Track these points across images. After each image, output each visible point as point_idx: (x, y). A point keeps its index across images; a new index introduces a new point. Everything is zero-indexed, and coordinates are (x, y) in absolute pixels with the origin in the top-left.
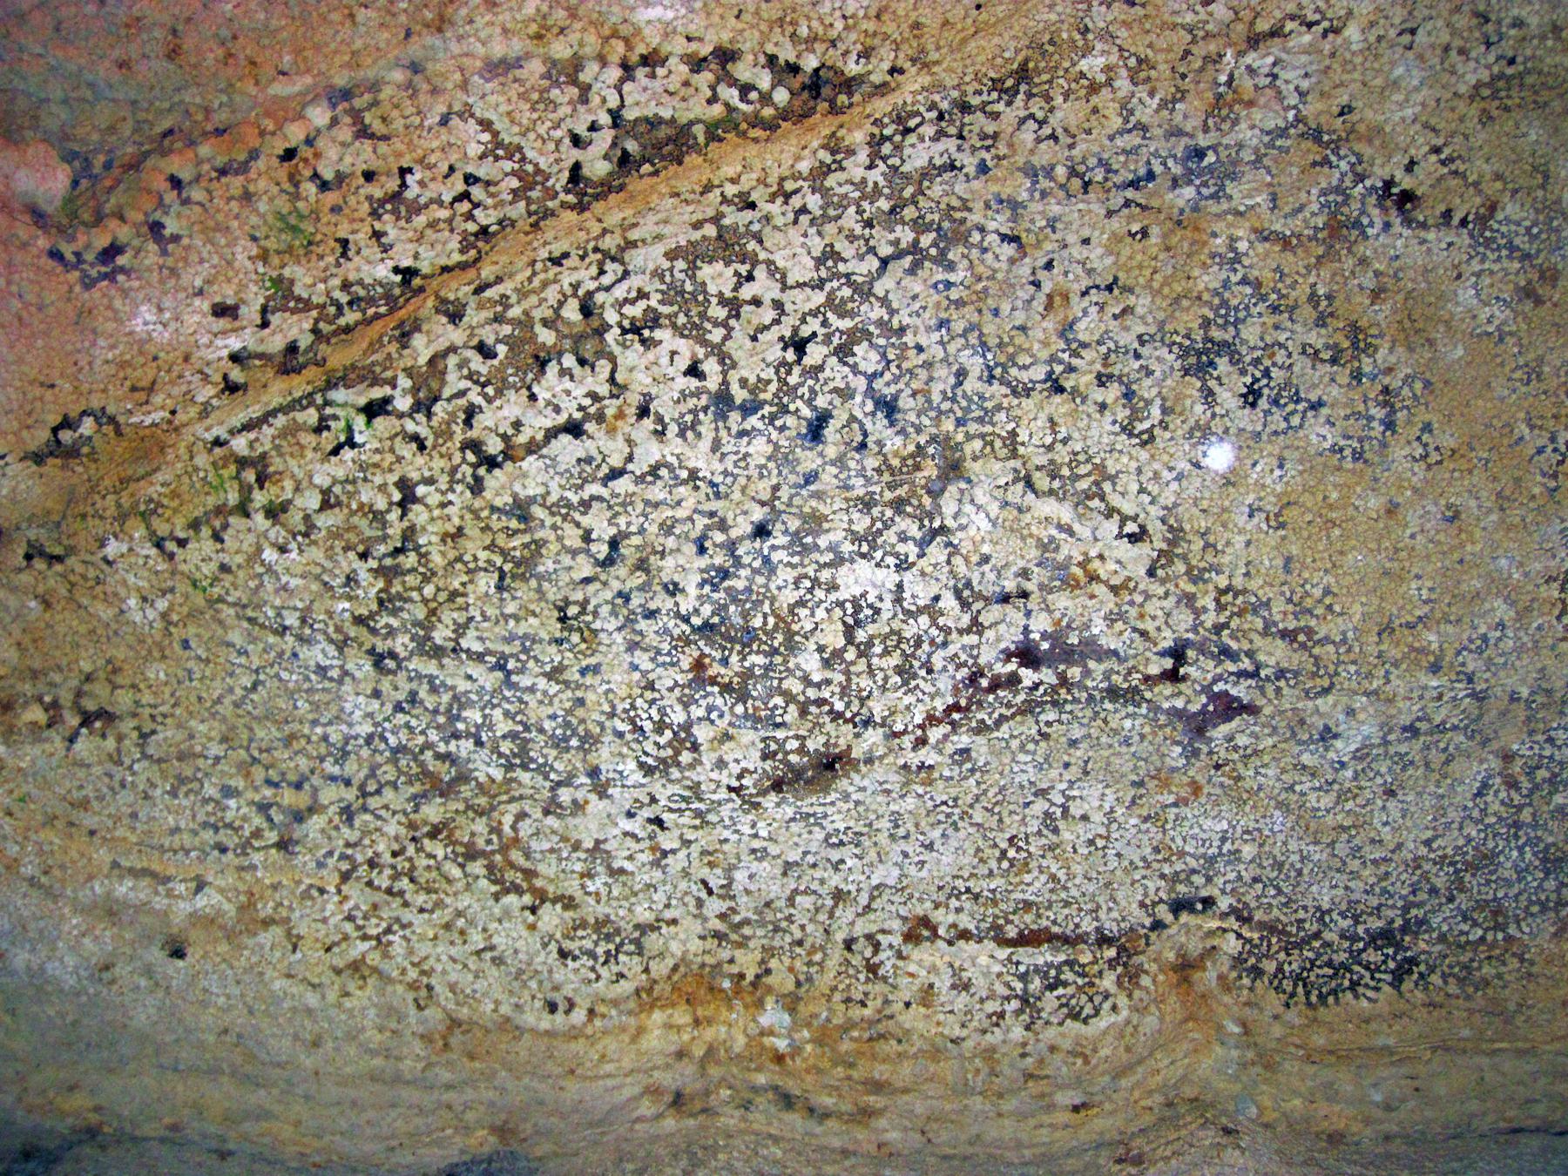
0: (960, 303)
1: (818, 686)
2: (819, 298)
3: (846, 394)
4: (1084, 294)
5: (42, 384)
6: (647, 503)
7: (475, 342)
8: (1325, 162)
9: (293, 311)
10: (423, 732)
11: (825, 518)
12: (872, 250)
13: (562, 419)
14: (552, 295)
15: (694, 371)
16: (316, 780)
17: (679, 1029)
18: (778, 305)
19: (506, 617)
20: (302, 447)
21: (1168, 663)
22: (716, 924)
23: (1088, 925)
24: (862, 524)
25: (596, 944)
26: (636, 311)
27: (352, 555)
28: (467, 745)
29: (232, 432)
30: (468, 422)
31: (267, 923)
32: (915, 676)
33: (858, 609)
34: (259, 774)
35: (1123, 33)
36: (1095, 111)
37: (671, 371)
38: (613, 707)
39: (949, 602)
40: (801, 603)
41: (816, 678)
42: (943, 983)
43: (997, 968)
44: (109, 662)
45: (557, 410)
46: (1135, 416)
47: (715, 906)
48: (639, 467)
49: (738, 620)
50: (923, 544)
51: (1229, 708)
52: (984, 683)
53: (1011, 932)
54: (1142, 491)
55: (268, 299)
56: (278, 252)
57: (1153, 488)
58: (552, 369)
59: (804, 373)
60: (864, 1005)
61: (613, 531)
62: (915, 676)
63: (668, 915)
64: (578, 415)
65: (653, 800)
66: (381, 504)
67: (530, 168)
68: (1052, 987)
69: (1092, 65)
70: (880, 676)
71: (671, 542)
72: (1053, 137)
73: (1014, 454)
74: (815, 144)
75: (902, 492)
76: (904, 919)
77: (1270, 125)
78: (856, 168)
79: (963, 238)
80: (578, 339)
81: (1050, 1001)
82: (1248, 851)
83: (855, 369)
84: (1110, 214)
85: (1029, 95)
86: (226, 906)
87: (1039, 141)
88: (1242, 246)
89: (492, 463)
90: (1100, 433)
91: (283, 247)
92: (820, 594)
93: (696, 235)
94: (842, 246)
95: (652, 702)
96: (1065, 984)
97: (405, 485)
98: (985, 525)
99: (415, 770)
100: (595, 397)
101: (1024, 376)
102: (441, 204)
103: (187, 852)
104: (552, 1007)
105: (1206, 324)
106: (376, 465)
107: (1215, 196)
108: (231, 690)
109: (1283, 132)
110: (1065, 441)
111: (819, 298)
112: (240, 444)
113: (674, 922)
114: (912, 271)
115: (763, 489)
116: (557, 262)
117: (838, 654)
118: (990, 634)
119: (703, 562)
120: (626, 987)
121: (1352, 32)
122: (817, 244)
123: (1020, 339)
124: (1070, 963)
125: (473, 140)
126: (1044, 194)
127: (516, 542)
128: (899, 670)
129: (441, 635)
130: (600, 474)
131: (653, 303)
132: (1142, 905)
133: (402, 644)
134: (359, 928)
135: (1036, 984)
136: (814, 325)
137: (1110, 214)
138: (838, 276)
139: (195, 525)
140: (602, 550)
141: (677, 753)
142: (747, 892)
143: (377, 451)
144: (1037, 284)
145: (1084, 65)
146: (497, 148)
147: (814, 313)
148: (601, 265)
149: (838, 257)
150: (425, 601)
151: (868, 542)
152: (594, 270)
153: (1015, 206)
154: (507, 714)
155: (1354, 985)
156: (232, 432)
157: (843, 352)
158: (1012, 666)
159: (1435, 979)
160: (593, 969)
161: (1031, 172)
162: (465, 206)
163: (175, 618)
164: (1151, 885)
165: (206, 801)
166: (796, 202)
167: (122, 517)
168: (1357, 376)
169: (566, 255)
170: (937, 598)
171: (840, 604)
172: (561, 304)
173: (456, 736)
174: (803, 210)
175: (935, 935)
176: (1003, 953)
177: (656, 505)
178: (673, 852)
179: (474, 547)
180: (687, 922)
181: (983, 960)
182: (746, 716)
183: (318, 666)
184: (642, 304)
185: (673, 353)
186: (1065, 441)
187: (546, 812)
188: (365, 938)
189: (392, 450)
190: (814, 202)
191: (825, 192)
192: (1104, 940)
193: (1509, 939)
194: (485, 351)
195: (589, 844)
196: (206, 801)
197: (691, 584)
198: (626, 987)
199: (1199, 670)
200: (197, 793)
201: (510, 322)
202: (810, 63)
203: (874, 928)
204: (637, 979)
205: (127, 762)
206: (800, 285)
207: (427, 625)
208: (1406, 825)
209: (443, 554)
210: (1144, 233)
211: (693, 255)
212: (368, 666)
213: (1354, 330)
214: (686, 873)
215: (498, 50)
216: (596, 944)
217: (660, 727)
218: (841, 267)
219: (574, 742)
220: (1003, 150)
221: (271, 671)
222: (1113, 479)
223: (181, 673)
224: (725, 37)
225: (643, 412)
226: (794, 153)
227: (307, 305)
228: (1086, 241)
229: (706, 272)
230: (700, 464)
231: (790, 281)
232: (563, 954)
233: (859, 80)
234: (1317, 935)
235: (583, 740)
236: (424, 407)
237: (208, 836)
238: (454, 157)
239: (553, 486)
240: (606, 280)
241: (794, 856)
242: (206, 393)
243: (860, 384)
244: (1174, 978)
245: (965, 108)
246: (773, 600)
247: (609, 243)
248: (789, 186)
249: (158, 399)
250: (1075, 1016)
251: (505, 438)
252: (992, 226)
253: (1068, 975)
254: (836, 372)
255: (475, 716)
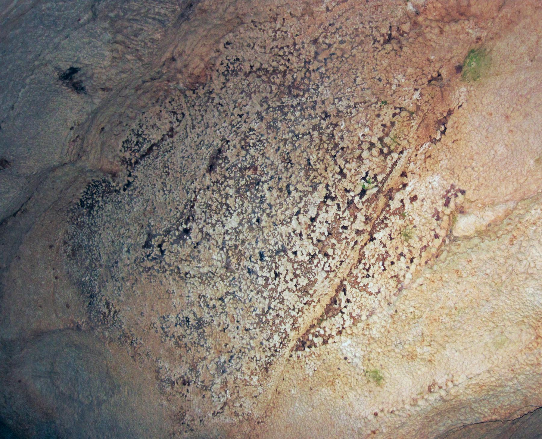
0: (251, 307)
1: (225, 187)
2: (279, 290)
3: (262, 268)
4: (228, 325)
5: (457, 140)
6: (289, 208)
7: (349, 228)
8: (202, 382)
9: (397, 209)
10: (307, 98)
11: (250, 232)
12: (273, 310)
13: (318, 220)
14: (338, 252)
15: (295, 253)
16: (323, 64)
17: (194, 69)
18: (287, 282)
19: (305, 151)
20: (378, 167)
21: (163, 248)
22: (213, 95)
23: (142, 162)
24: (241, 236)
25: (234, 67)
26: (316, 261)
27: (345, 146)
28: (295, 103)
29: (399, 159)
30: (338, 205)
31: (303, 15)
32: (206, 208)
33: (230, 213)
34: (339, 53)
35: (254, 389)
36: (249, 369)
37: (301, 249)
38: (268, 142)
39: (211, 231)
40: (242, 205)
41: (227, 188)
42: (158, 123)
43: (151, 136)
44: (400, 56)
45: (320, 222)
46: (205, 300)
47: (216, 101)
48: (294, 218)
49: (253, 190)
50: (224, 242)
51: (147, 245)
52: (191, 218)
53: (154, 148)
54: (193, 284)
55: (404, 209)
56: (407, 225)
57: (193, 286)
58: (326, 233)
59: (272, 268)
60: (170, 102)
61: (292, 195)
62: (206, 208)
63: (224, 90)
64: (315, 224)
65: (245, 122)
66: (347, 165)
67: (357, 286)
68: (137, 142)
69: (255, 379)
70: (215, 200)
71: (278, 201)
72: (253, 358)
73: (220, 277)
74: (302, 326)
75: (237, 251)
76: (177, 132)
77: (215, 385)
78: (288, 327)
79: (257, 324)
80: (324, 246)
81: (135, 139)
82: (127, 207)
83: (262, 276)
84: (233, 347)
85: (262, 365)
86: (317, 9)
87: (255, 356)
88: (208, 353)
89: (326, 197)
90: (209, 293)
91: (408, 228)
92: (240, 211)
93: (314, 288)
94: (281, 306)
95: (260, 150)
96: (136, 145)
97: (344, 176)
98: (215, 257)
99: (302, 87)
100: (313, 231)
101: (229, 297)
102: (373, 264)
103: (339, 16)
104: (228, 43)
105: (204, 331)
106: (355, 175)
107: (217, 362)
108: (361, 73)
109: (213, 385)
110: (213, 286)
111: (279, 290)
112: (395, 156)
113: (222, 89)
114: (263, 309)
115: (266, 231)
116: (342, 262)
117: (227, 198)
118: (197, 230)
119: (268, 201)
120: (218, 63)
121: (211, 415)
122: (286, 303)
123: (235, 306)
124: (139, 151)
125: (373, 289)
126: (247, 344)
127: (312, 175)
128: (210, 206)
129: (316, 134)
130: (302, 210)
131: (313, 266)
132: (136, 177)
133: (324, 124)
134: (282, 31)
135: (141, 140)
136: (276, 282)
137: (233, 347)
138: (278, 298)
139: (393, 124)
140: (292, 188)
141: (245, 142)
142: (212, 111)
143: (357, 180)
144: (238, 322)
145: (257, 377)
146: (365, 289)
147: (278, 285)
148: (331, 268)
149: (279, 303)
150: (325, 142)
151: (238, 232)
152: (332, 265)
153: (252, 338)
154: (290, 120)
155: (87, 193)
156: (399, 159)
157: (267, 279)
158: (188, 226)
159: (76, 206)
160: (229, 60)
161: (253, 348)
162: (367, 267)
163: (388, 85)
164: (138, 183)
165: (346, 34)
166: (297, 310)
167: (418, 108)
168: (174, 336)
169: (340, 265)
170: (214, 230)
171: (235, 211)
172: (334, 252)
173: (299, 104)
174: (294, 310)
175: (167, 134)
176: (152, 142)
177: (286, 210)
178: (234, 109)
179: (320, 166)
180: (219, 91)
181: (155, 136)
182: (237, 165)
183: (342, 100)
184: (315, 264)
185: (302, 255)
186: (213, 286)
187: (266, 97)
188: (279, 29)
189: (353, 183)
190: (293, 313)
191: (292, 317)
192: (137, 162)
193: (74, 224)
194: (344, 227)
195: (253, 95)
196: (346, 34)
197: (268, 194)
198: (218, 63)
199: (156, 251)
200: (350, 34)
201: (343, 239)
202: (307, 349)
203: (181, 124)
204: (218, 66)
205: (374, 29)
206: (285, 290)
207: (321, 134)
208: (107, 236)
209: (327, 160)
210: (226, 346)
211: (311, 283)
212: (328, 110)
213: (180, 347)
214: (228, 104)
215: (375, 317)
216: (234, 67)
217: (254, 145)
218: (278, 301)
219: (272, 123)
220: (261, 349)
221: (354, 88)
222: (200, 283)
223: (378, 68)
224: (328, 346)
225: (301, 235)
226: (304, 322)
227: (394, 214)
228: (234, 338)
229: (306, 281)
230: (282, 228)
231: (287, 290)
232: (238, 59)
233: (297, 350)
234: (102, 197)
235: (270, 125)
236: (350, 203)
237: (338, 25)
238: (374, 280)
239: (312, 199)
240: (327, 265)
241: (208, 130)
242: (412, 166)
243: (260, 273)
244: (114, 171)
245: (273, 355)
246: (249, 202)
247: (332, 275)
248: (300, 313)
249: (423, 157)
250: (127, 141)
251: (328, 206)
252: (254, 330)
253: (137, 147)
254: (266, 273)
255: (298, 114)
